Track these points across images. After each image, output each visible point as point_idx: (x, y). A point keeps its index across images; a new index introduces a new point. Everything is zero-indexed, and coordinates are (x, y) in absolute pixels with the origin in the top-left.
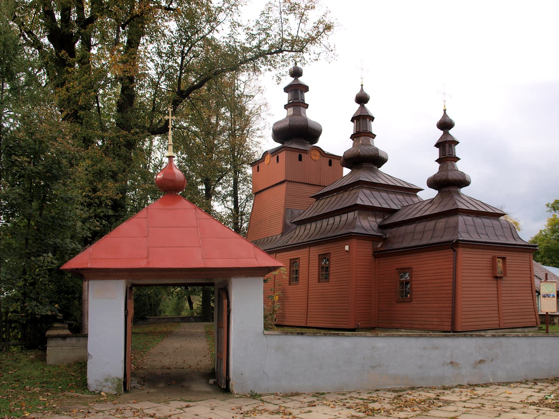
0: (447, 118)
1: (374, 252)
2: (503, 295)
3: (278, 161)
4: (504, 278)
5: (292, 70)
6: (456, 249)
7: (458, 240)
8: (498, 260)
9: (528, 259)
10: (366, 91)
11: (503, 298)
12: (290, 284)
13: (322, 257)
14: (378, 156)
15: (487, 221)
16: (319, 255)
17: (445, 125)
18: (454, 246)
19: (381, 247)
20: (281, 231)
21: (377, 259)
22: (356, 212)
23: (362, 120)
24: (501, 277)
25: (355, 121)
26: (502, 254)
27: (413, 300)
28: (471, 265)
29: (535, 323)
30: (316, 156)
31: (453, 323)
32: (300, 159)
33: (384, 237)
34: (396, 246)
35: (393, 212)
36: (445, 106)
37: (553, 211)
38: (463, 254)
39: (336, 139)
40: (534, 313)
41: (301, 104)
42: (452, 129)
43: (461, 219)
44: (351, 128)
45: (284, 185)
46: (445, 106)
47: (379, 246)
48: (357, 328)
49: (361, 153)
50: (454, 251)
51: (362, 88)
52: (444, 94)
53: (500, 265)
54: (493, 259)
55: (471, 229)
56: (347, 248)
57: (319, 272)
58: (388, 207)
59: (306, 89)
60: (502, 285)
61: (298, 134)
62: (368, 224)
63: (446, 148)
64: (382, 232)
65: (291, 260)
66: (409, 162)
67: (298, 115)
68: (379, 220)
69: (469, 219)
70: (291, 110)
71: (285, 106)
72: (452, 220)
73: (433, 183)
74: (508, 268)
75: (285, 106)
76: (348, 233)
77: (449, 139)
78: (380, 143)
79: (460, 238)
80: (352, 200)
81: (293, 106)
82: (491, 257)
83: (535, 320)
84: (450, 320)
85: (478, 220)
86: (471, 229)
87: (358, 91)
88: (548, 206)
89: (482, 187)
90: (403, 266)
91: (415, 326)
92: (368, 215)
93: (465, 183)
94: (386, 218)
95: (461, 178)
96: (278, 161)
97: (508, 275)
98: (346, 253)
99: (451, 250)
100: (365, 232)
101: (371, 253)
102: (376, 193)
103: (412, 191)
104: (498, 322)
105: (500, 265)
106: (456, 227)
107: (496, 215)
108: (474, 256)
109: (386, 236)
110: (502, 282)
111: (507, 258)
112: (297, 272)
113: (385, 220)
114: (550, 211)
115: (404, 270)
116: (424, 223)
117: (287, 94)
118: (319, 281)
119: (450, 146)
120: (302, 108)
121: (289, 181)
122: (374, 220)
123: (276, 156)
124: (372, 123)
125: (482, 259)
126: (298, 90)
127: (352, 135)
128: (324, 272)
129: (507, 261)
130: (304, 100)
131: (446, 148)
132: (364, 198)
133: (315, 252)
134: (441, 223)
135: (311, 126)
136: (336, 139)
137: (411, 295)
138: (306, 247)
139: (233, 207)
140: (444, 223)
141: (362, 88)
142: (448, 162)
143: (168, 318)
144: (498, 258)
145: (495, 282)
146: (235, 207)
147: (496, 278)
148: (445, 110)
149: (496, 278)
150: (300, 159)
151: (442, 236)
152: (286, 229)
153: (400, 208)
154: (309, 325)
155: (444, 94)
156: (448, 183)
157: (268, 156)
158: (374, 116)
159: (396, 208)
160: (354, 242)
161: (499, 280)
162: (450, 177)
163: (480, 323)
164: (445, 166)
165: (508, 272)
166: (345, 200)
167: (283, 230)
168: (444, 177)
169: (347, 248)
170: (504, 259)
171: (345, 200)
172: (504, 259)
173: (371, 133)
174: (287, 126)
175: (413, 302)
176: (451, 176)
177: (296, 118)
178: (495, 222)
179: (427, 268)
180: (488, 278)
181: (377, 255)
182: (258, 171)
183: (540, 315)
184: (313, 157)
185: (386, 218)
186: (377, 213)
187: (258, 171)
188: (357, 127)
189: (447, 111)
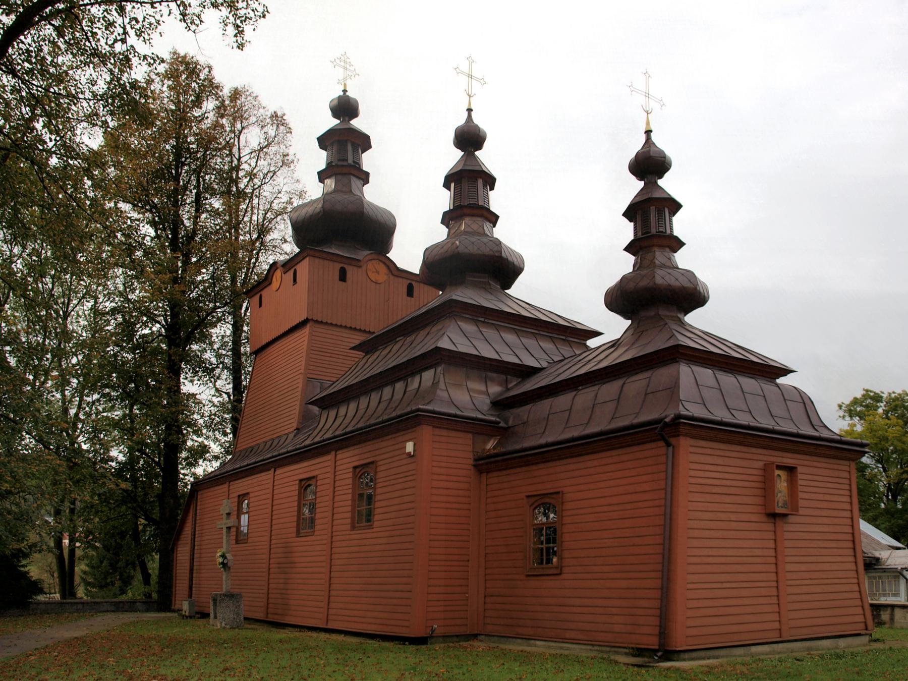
0: (652, 149)
1: (476, 460)
2: (788, 559)
3: (295, 280)
4: (791, 519)
5: (336, 102)
6: (673, 441)
7: (679, 417)
8: (777, 472)
9: (846, 475)
10: (477, 120)
11: (789, 567)
12: (298, 534)
13: (360, 471)
14: (501, 257)
15: (749, 383)
16: (355, 468)
17: (649, 165)
18: (668, 431)
19: (494, 448)
20: (295, 425)
21: (484, 476)
22: (439, 369)
23: (469, 186)
24: (785, 515)
25: (453, 185)
26: (788, 460)
27: (565, 570)
28: (710, 487)
29: (862, 626)
30: (382, 275)
31: (664, 632)
32: (343, 276)
33: (502, 424)
34: (527, 444)
35: (527, 372)
36: (648, 123)
37: (848, 418)
38: (692, 455)
39: (418, 232)
40: (858, 602)
41: (355, 172)
42: (667, 175)
43: (685, 372)
44: (444, 200)
45: (307, 330)
46: (648, 123)
47: (490, 445)
48: (431, 637)
49: (462, 250)
50: (668, 445)
51: (470, 116)
52: (647, 95)
53: (782, 485)
54: (767, 469)
55: (710, 395)
56: (410, 447)
57: (353, 506)
58: (517, 361)
59: (363, 142)
60: (787, 535)
61: (345, 229)
62: (470, 397)
63: (651, 218)
64: (498, 416)
65: (301, 481)
66: (567, 259)
67: (345, 192)
68: (495, 389)
69: (706, 374)
70: (330, 183)
71: (320, 173)
72: (661, 375)
73: (621, 299)
74: (801, 495)
75: (320, 173)
76: (412, 412)
77: (657, 195)
78: (509, 233)
79: (684, 412)
80: (433, 340)
81: (336, 174)
82: (760, 464)
83: (861, 619)
84: (655, 621)
85: (728, 380)
86: (710, 395)
87: (461, 120)
88: (840, 406)
89: (744, 282)
90: (547, 488)
91: (568, 635)
92: (468, 377)
93: (693, 297)
94: (510, 386)
95: (687, 284)
96: (295, 280)
97: (801, 512)
98: (410, 460)
99: (662, 443)
100: (453, 411)
101: (472, 462)
102: (489, 333)
103: (577, 335)
104: (777, 625)
105: (782, 485)
106: (673, 389)
107: (770, 372)
108: (720, 461)
109: (506, 422)
110: (787, 527)
111: (800, 469)
112: (313, 508)
113: (508, 390)
114: (844, 417)
115: (546, 501)
116: (596, 388)
117: (324, 154)
118: (353, 528)
119: (660, 213)
120: (353, 179)
121: (317, 322)
122: (482, 388)
123: (292, 271)
124: (491, 193)
125: (736, 468)
126: (346, 141)
127: (445, 214)
128: (364, 510)
129: (800, 476)
130: (359, 164)
131: (651, 218)
132: (456, 338)
133: (348, 458)
134: (636, 384)
135: (371, 212)
136: (418, 232)
137: (561, 559)
138: (327, 453)
139: (229, 388)
140: (644, 382)
141: (470, 116)
142: (656, 249)
143: (83, 603)
144: (779, 467)
145: (770, 527)
146: (234, 388)
147: (774, 516)
148: (648, 132)
149: (774, 516)
150: (343, 276)
151: (637, 414)
152: (306, 420)
153: (545, 365)
154: (331, 626)
155: (647, 95)
156: (655, 293)
157: (278, 273)
158: (495, 174)
159: (537, 365)
160: (426, 431)
161: (779, 522)
162: (659, 281)
163: (734, 628)
164: (649, 256)
165: (801, 503)
166: (420, 344)
167: (299, 423)
168: (644, 283)
169: (410, 447)
170: (791, 470)
171: (420, 344)
172: (791, 470)
173: (488, 210)
174: (318, 210)
175: (563, 576)
176: (662, 278)
177: (339, 197)
178: (768, 387)
179: (595, 493)
180: (754, 518)
181: (485, 465)
182: (260, 305)
183: (872, 605)
184: (373, 276)
185: (510, 386)
186: (490, 374)
187: (260, 305)
188: (456, 197)
189: (654, 137)
